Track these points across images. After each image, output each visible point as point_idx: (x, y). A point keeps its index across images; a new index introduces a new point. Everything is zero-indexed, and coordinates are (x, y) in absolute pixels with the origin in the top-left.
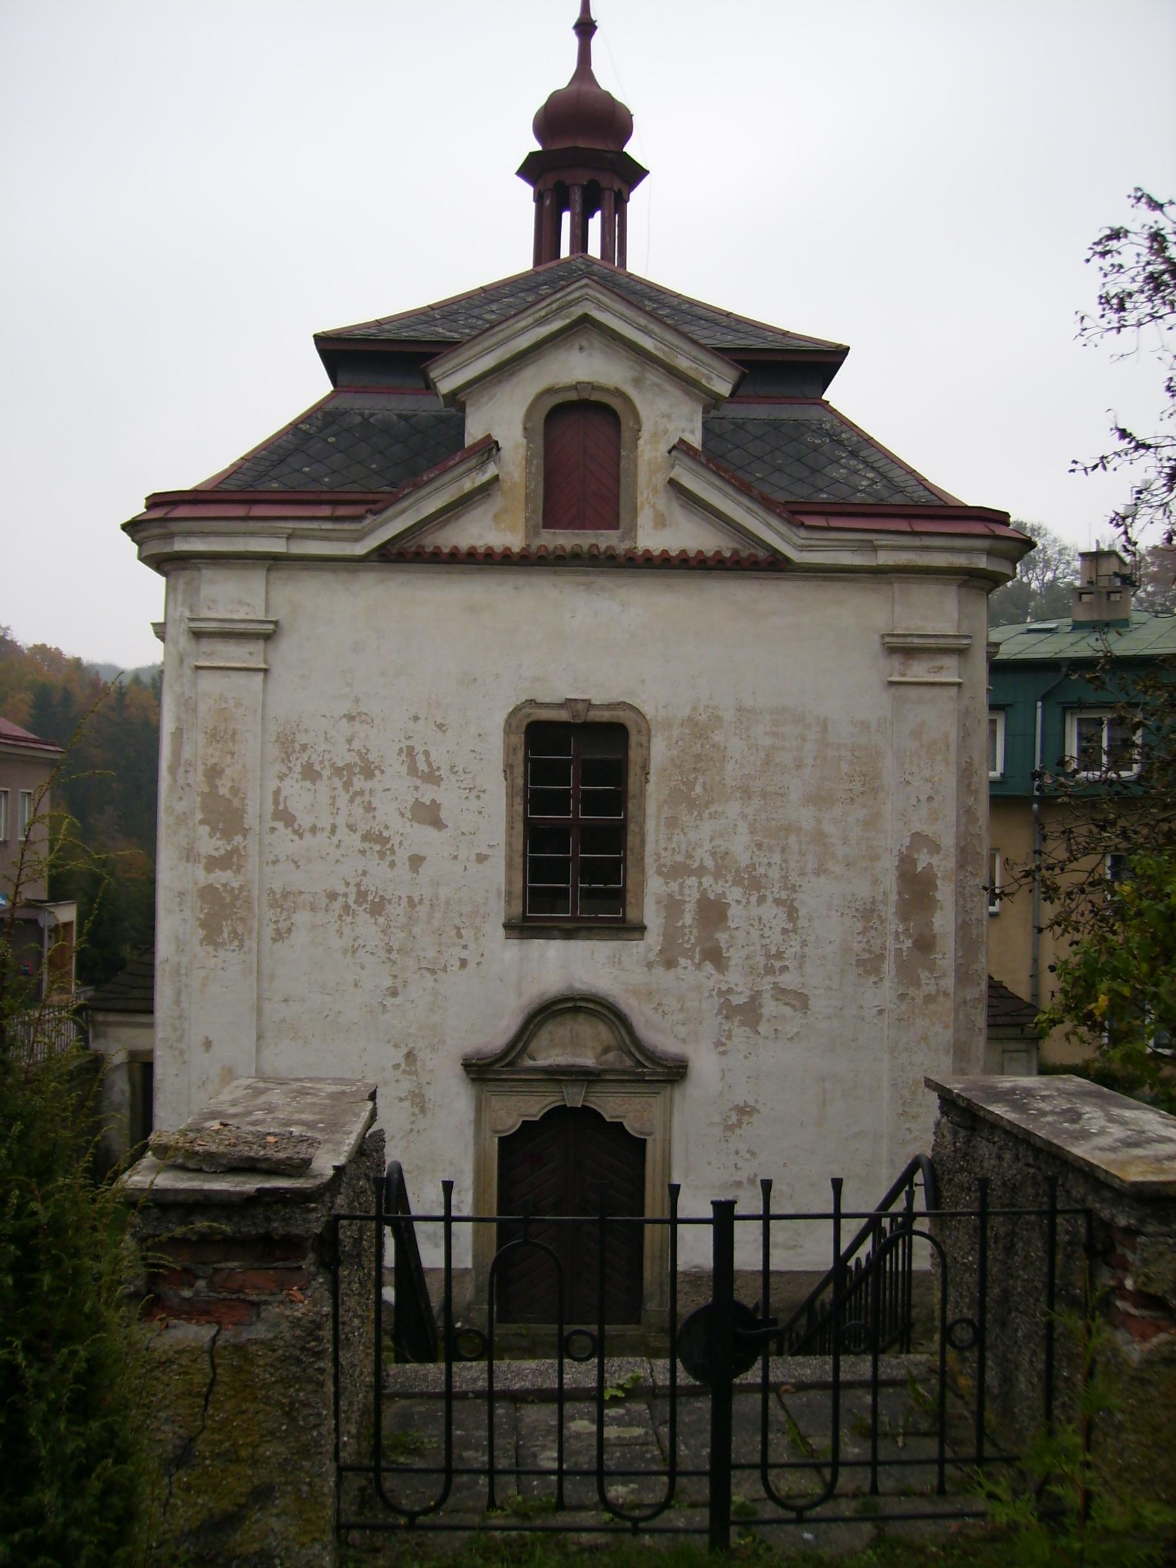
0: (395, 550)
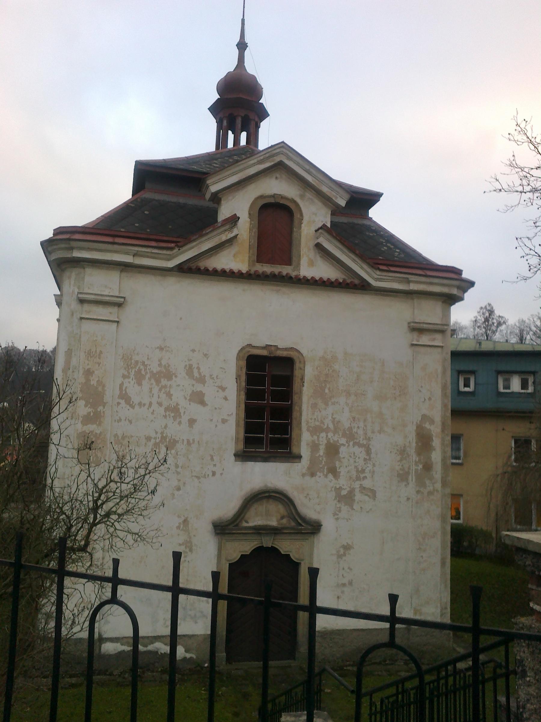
0: (186, 267)
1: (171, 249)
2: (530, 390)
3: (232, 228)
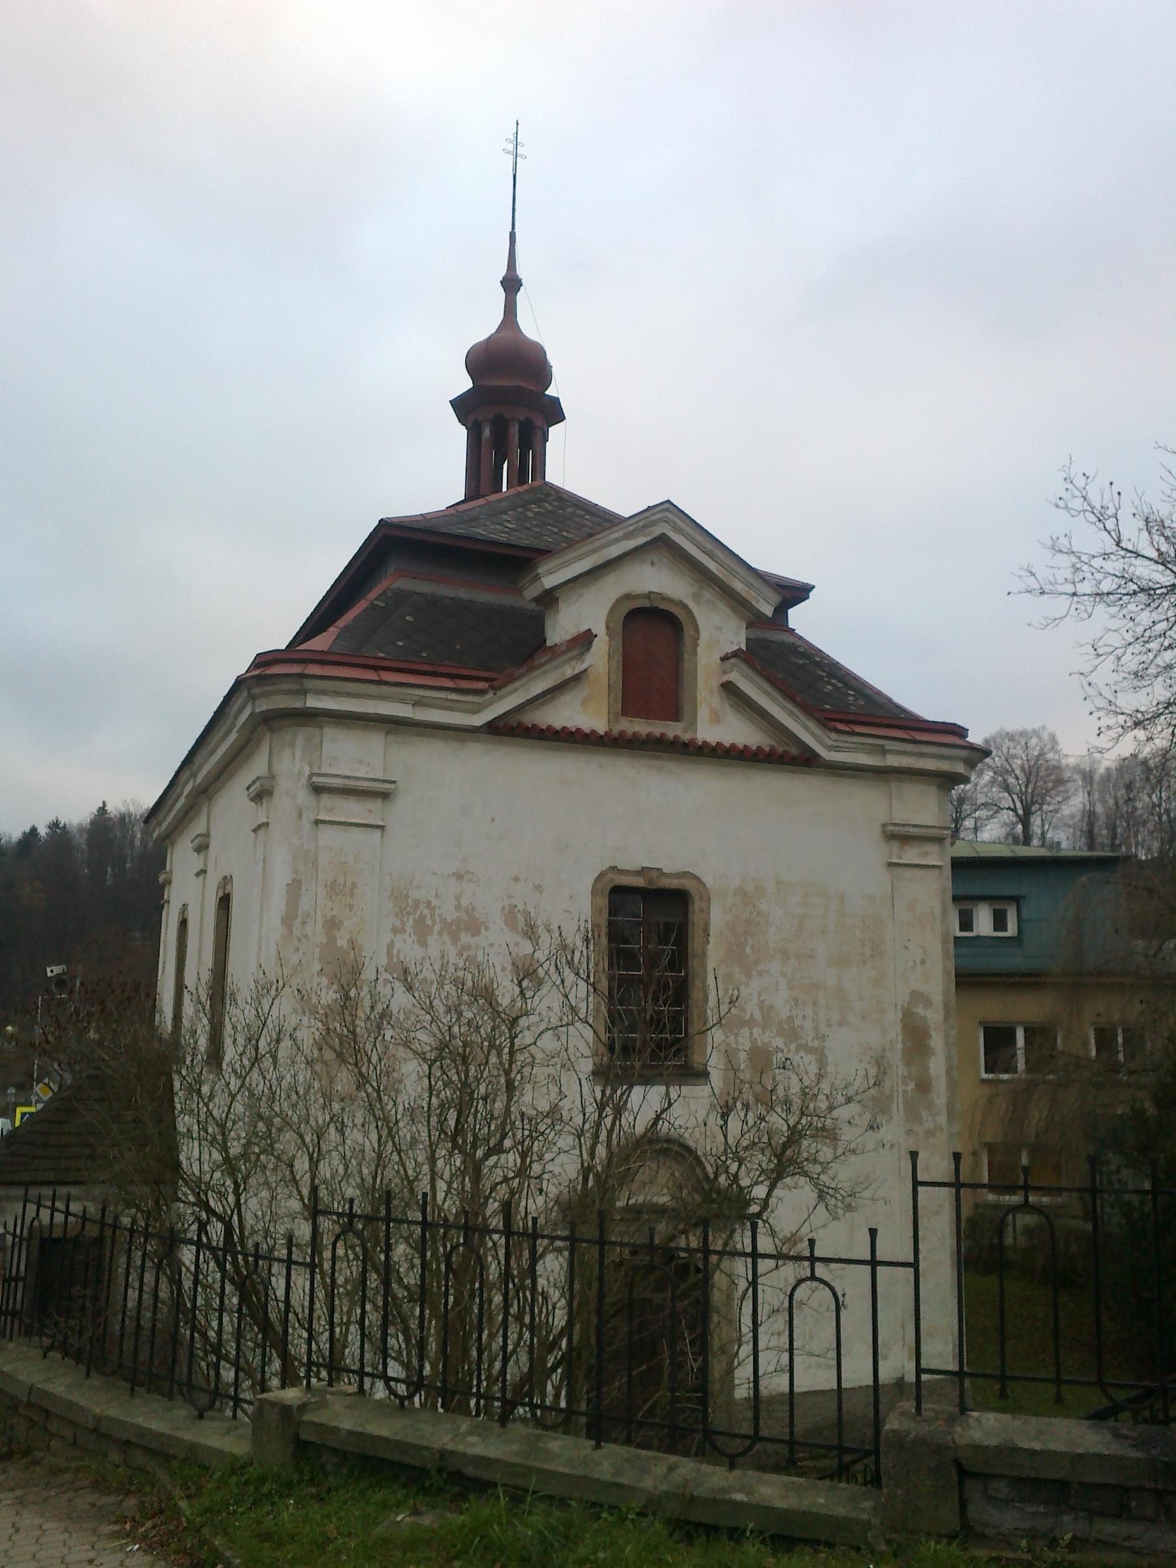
0: (501, 724)
1: (481, 692)
2: (1012, 930)
3: (581, 656)
